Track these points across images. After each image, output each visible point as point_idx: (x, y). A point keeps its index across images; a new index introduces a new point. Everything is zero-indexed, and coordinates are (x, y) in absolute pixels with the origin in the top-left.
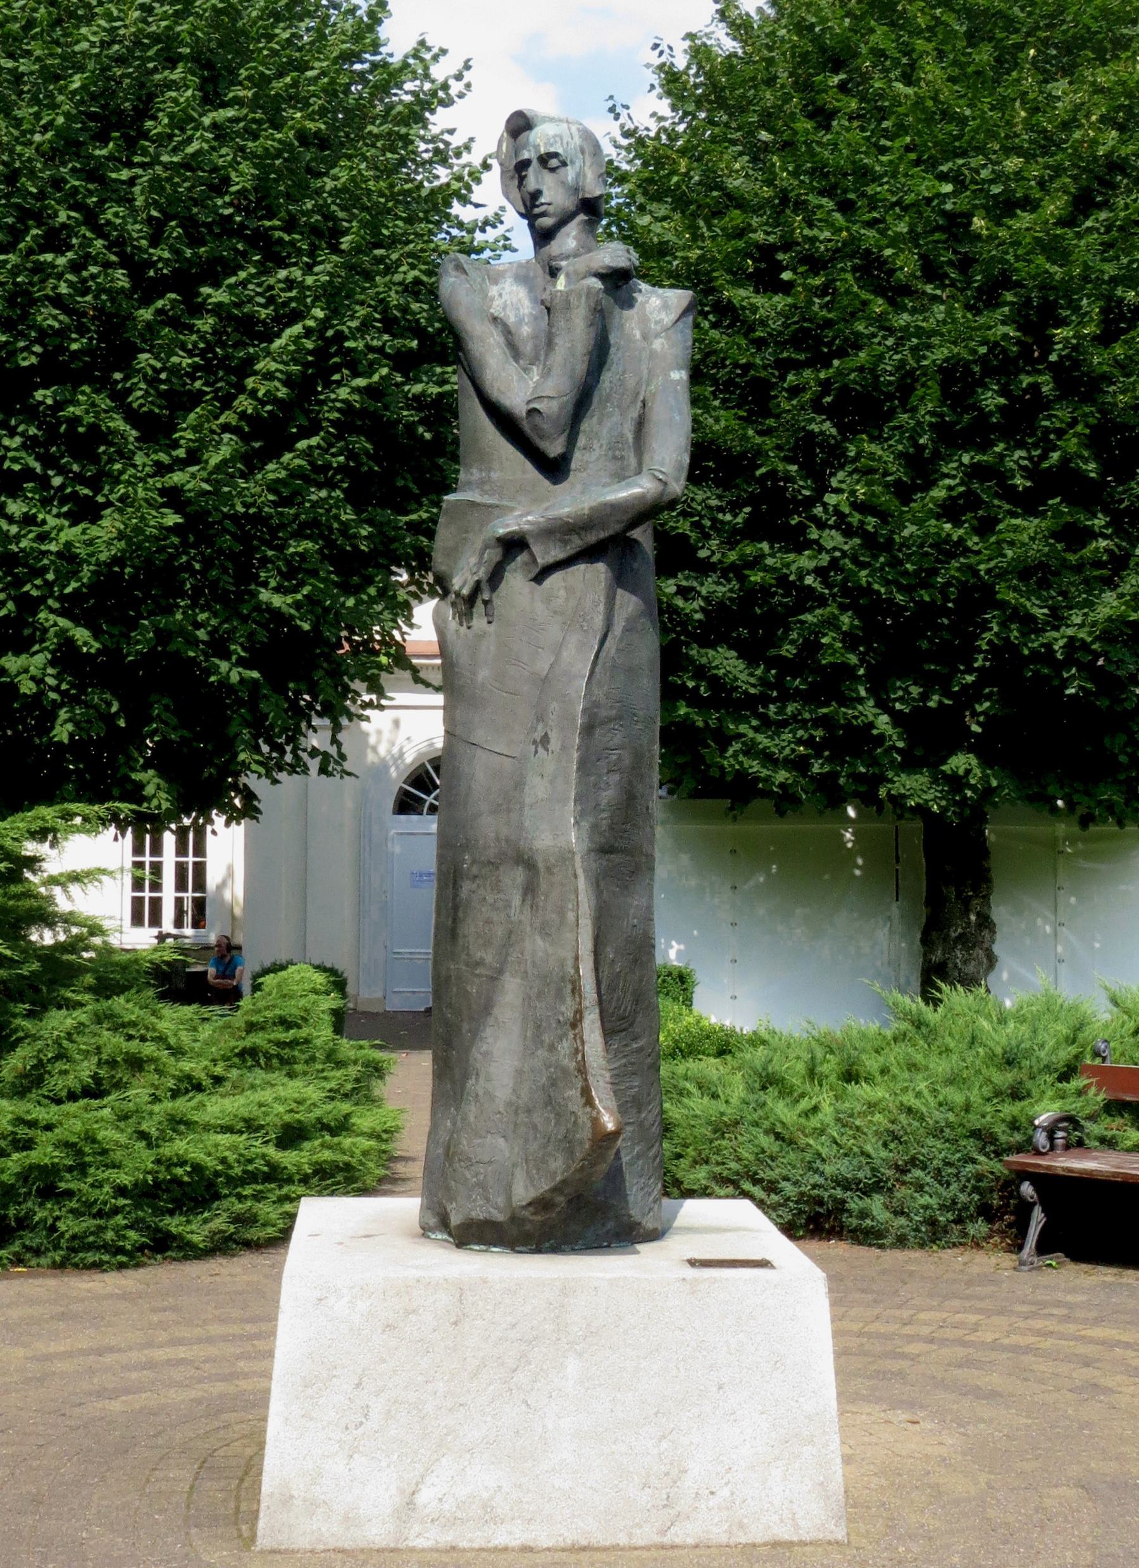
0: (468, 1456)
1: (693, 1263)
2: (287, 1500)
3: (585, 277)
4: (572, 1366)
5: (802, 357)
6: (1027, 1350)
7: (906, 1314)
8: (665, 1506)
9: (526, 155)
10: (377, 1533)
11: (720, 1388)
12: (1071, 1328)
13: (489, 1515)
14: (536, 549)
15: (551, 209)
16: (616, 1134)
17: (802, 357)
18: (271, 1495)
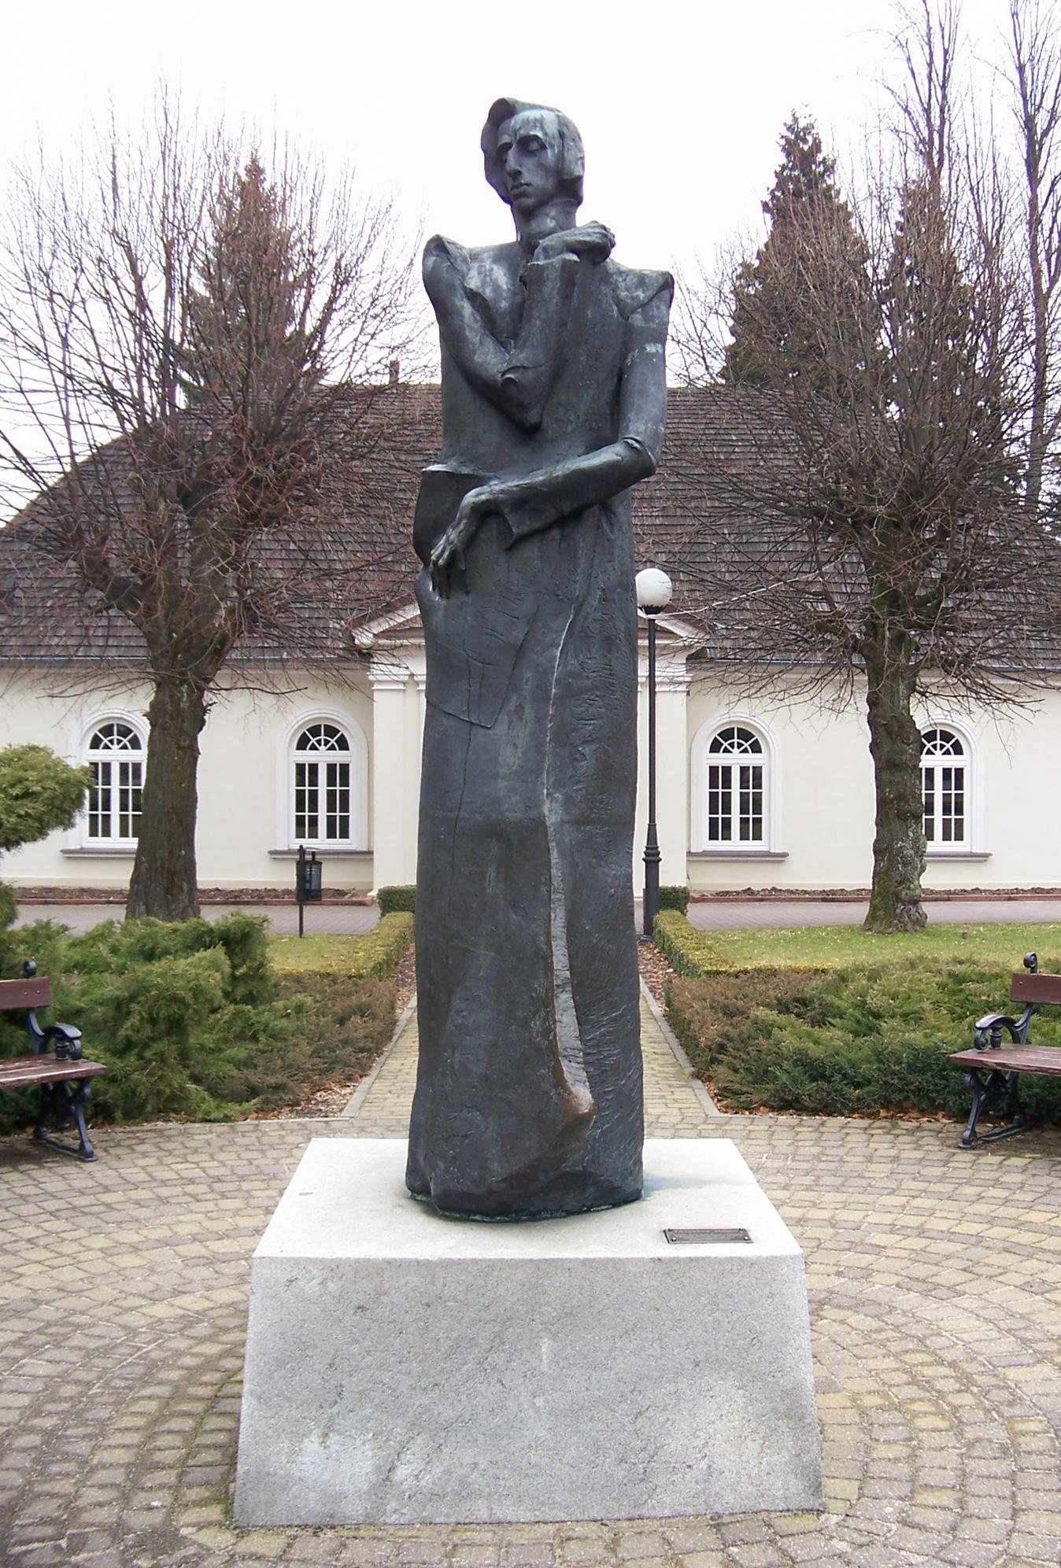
0: (443, 1434)
1: (673, 1236)
3: (561, 253)
5: (87, 792)
9: (506, 139)
11: (697, 1365)
12: (1011, 1212)
14: (511, 519)
15: (529, 189)
16: (586, 1118)
17: (87, 792)
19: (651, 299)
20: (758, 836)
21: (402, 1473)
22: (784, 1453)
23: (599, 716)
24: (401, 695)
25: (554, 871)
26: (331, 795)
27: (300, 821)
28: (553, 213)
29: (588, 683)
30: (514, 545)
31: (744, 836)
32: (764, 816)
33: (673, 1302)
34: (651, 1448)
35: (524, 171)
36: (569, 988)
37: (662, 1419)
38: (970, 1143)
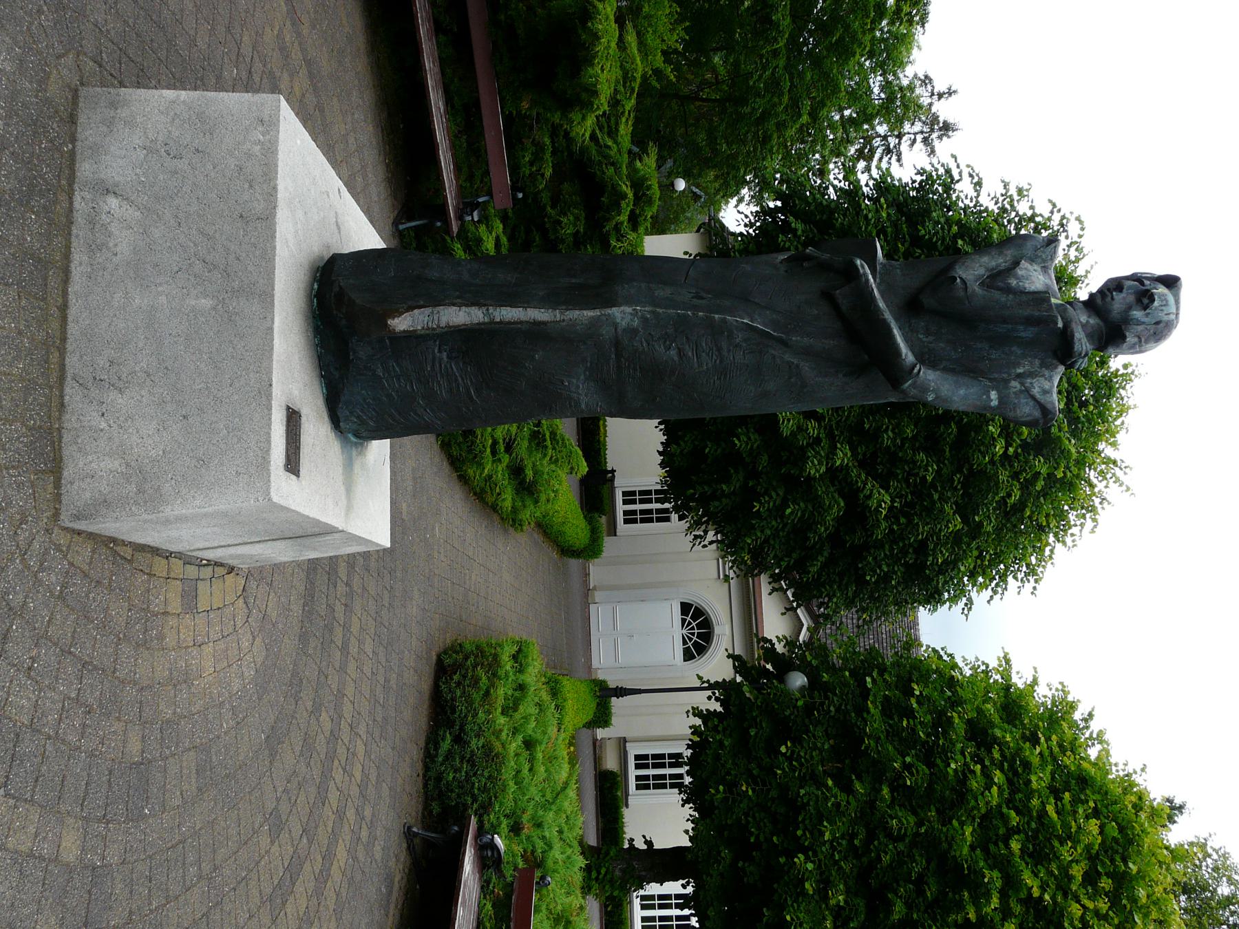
2: (113, 105)
4: (206, 303)
6: (322, 798)
7: (362, 730)
8: (95, 378)
10: (85, 169)
13: (94, 248)
15: (1109, 299)
18: (118, 95)
19: (1033, 398)
20: (638, 787)
21: (113, 202)
22: (108, 489)
23: (700, 365)
24: (716, 575)
25: (577, 312)
26: (663, 777)
27: (633, 493)
28: (1092, 321)
29: (725, 353)
30: (827, 296)
31: (638, 778)
32: (652, 791)
33: (236, 397)
34: (121, 384)
35: (1123, 295)
36: (486, 320)
37: (143, 393)
38: (408, 834)
